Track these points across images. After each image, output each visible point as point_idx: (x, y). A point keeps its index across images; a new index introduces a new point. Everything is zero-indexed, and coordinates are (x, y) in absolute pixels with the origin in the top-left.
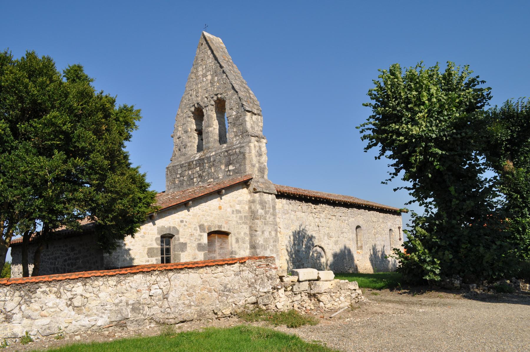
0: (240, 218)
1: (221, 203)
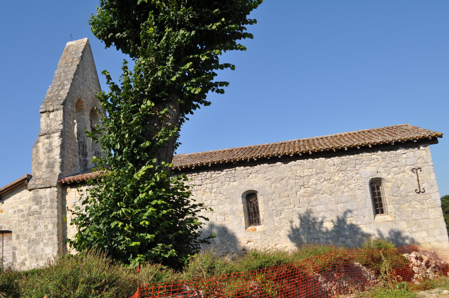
0: (21, 217)
1: (2, 207)
